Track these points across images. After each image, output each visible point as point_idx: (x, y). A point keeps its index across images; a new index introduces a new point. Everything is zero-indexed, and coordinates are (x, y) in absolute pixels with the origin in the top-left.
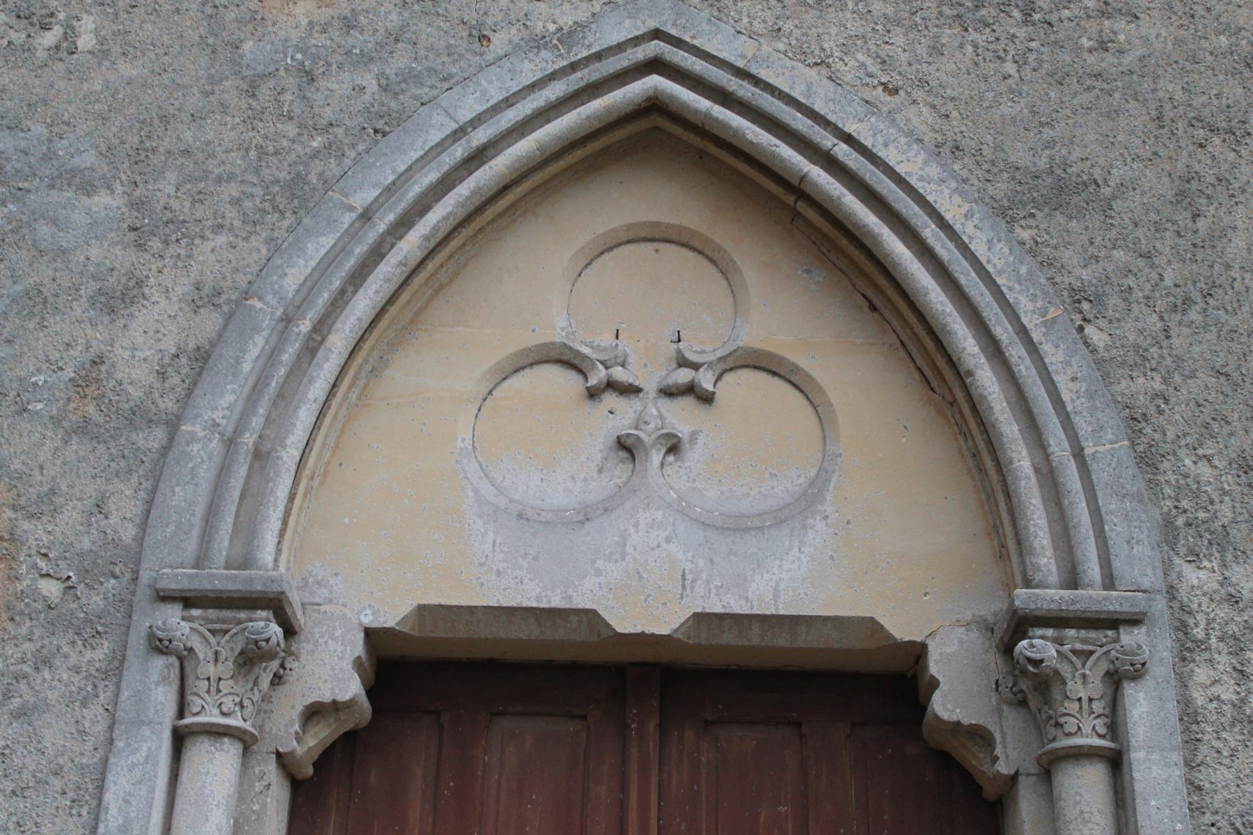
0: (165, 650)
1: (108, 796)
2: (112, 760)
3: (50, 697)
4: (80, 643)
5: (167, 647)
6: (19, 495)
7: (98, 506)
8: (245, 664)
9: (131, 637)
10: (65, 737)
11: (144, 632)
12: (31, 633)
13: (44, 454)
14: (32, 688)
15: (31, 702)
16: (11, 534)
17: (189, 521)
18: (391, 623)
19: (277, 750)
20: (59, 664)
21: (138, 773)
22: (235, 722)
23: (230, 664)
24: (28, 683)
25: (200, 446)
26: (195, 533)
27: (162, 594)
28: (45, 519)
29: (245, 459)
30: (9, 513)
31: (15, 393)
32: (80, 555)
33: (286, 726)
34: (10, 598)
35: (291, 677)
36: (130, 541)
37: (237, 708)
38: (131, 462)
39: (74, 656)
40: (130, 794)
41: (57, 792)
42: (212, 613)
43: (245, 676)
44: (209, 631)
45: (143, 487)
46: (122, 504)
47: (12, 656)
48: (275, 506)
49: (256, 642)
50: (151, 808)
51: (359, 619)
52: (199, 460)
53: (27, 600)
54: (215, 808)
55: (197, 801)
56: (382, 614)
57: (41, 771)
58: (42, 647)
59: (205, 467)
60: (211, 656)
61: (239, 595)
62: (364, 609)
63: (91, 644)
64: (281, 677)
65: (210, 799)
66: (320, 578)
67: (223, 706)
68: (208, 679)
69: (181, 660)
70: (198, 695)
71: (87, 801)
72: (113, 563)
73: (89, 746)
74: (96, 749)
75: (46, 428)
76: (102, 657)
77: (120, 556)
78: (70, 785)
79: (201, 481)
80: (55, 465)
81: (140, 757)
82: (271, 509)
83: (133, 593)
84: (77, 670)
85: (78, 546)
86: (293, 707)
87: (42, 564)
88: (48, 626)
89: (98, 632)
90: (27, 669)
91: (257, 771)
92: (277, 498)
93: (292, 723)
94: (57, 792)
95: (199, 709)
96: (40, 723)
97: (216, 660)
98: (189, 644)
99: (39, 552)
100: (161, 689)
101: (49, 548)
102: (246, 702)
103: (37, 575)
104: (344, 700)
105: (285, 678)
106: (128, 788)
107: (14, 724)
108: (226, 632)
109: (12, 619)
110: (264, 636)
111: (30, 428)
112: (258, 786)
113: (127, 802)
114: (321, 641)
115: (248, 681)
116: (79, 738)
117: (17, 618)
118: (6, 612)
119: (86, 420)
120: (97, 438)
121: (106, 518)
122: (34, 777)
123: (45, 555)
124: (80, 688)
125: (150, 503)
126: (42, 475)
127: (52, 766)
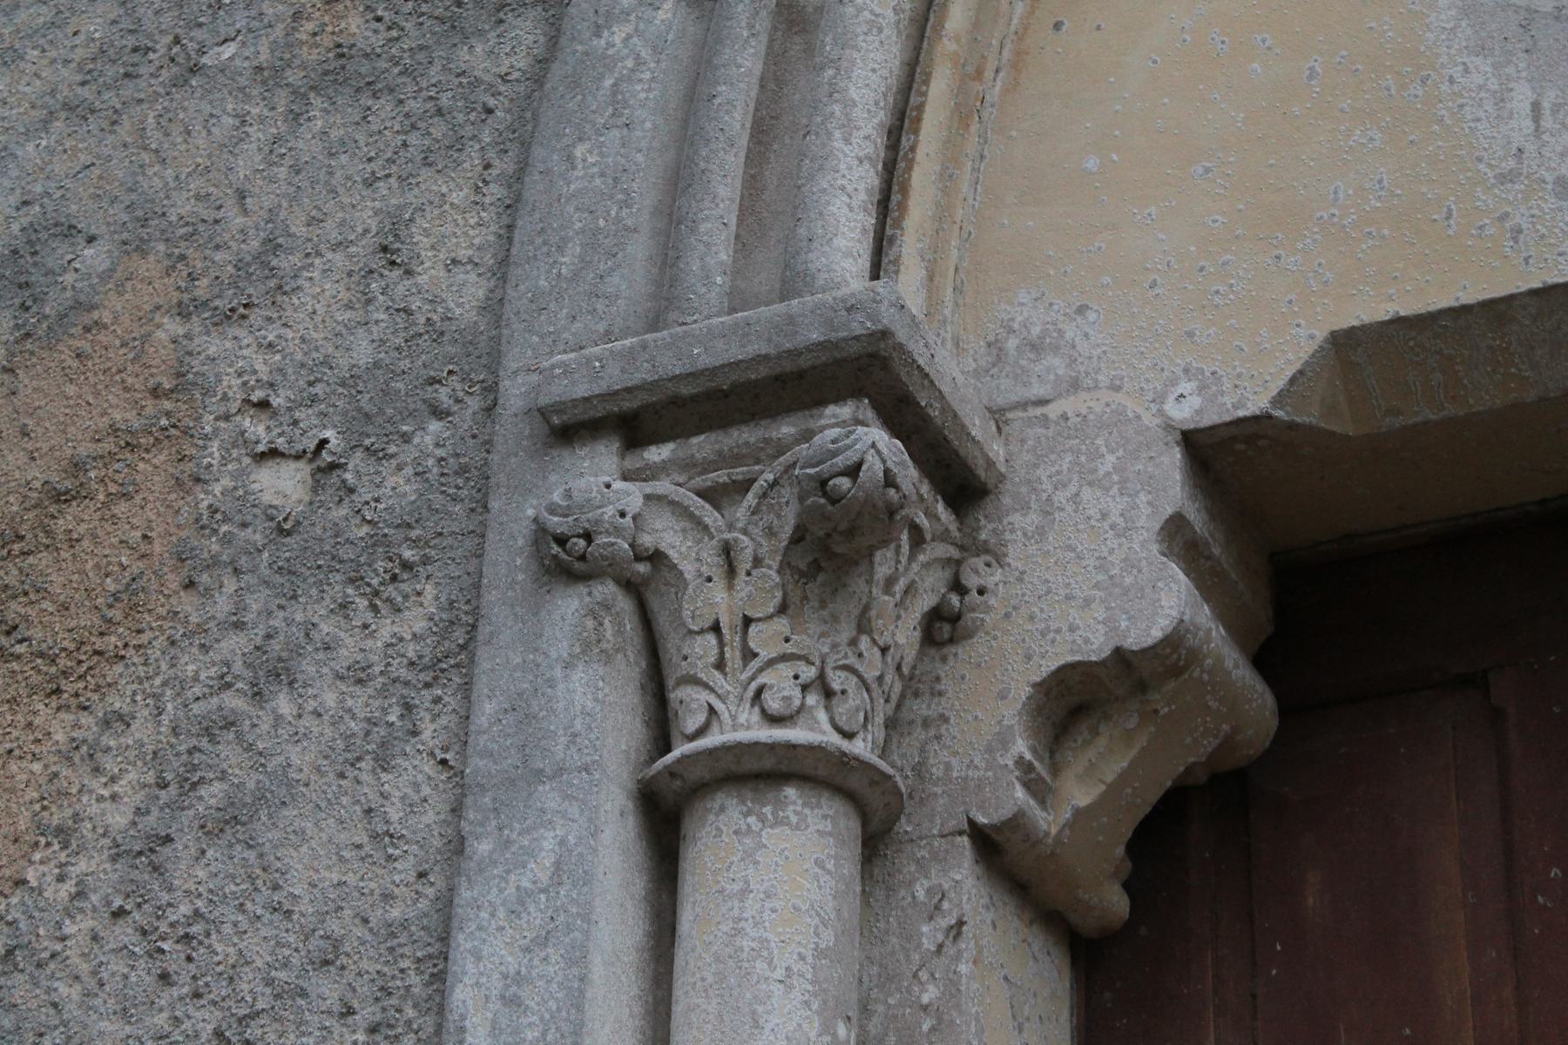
0: (578, 566)
1: (462, 995)
2: (465, 894)
3: (295, 760)
4: (362, 603)
5: (582, 558)
6: (192, 277)
7: (385, 249)
8: (816, 567)
9: (490, 555)
10: (341, 859)
11: (521, 535)
12: (241, 607)
13: (247, 162)
14: (249, 748)
15: (251, 785)
16: (180, 375)
17: (618, 219)
18: (1257, 403)
19: (971, 822)
20: (312, 669)
21: (535, 916)
22: (814, 731)
23: (771, 573)
24: (239, 736)
25: (629, 28)
26: (639, 249)
27: (556, 420)
28: (256, 317)
29: (751, 26)
30: (174, 326)
31: (169, 39)
32: (351, 382)
33: (990, 750)
34: (184, 534)
35: (988, 614)
36: (473, 316)
37: (812, 699)
38: (461, 118)
39: (349, 641)
40: (519, 979)
41: (329, 1012)
42: (702, 445)
43: (823, 604)
44: (699, 494)
45: (495, 172)
46: (449, 228)
47: (196, 679)
48: (848, 127)
49: (823, 483)
50: (580, 1009)
51: (1161, 412)
52: (630, 63)
53: (224, 528)
54: (777, 989)
55: (721, 977)
56: (1227, 385)
57: (286, 965)
58: (268, 637)
59: (647, 75)
60: (711, 560)
61: (763, 371)
62: (1174, 382)
63: (389, 600)
64: (955, 619)
65: (760, 965)
66: (1036, 330)
67: (766, 696)
68: (716, 628)
69: (634, 588)
70: (695, 681)
71: (409, 1023)
72: (433, 381)
73: (406, 868)
74: (422, 875)
75: (248, 98)
76: (420, 626)
77: (451, 360)
78: (364, 989)
79: (640, 113)
80: (272, 180)
81: (540, 869)
82: (837, 134)
83: (488, 447)
84: (358, 675)
85: (344, 362)
86: (1002, 696)
87: (258, 430)
88: (278, 579)
89: (407, 566)
90: (233, 701)
91: (921, 894)
92: (850, 104)
93: (1003, 740)
94: (329, 1012)
95: (701, 718)
96: (275, 835)
97: (731, 571)
98: (647, 540)
99: (247, 401)
100: (579, 675)
101: (271, 385)
102: (837, 680)
103: (247, 460)
104: (1149, 642)
105: (969, 617)
106: (512, 963)
107: (210, 853)
108: (745, 486)
109: (190, 585)
110: (840, 461)
111: (208, 109)
112: (929, 934)
113: (512, 1002)
114: (1061, 497)
115: (835, 619)
116: (378, 856)
117: (205, 578)
118: (174, 569)
119: (341, 52)
120: (371, 87)
121: (409, 273)
122: (269, 982)
123: (264, 405)
124: (368, 720)
125: (511, 207)
126: (245, 212)
127: (314, 943)
